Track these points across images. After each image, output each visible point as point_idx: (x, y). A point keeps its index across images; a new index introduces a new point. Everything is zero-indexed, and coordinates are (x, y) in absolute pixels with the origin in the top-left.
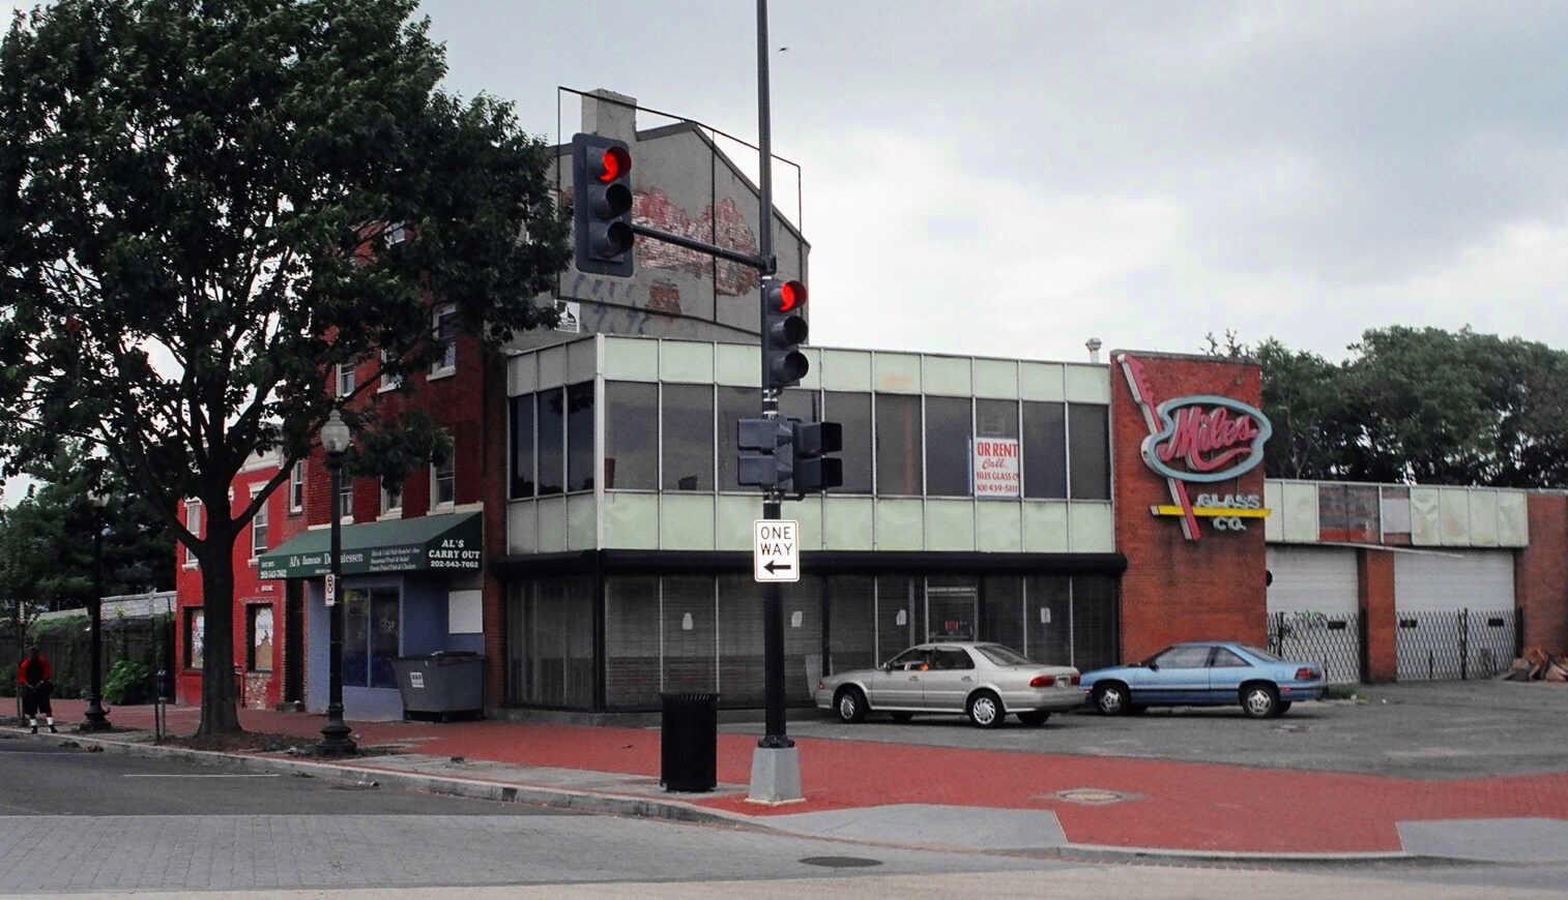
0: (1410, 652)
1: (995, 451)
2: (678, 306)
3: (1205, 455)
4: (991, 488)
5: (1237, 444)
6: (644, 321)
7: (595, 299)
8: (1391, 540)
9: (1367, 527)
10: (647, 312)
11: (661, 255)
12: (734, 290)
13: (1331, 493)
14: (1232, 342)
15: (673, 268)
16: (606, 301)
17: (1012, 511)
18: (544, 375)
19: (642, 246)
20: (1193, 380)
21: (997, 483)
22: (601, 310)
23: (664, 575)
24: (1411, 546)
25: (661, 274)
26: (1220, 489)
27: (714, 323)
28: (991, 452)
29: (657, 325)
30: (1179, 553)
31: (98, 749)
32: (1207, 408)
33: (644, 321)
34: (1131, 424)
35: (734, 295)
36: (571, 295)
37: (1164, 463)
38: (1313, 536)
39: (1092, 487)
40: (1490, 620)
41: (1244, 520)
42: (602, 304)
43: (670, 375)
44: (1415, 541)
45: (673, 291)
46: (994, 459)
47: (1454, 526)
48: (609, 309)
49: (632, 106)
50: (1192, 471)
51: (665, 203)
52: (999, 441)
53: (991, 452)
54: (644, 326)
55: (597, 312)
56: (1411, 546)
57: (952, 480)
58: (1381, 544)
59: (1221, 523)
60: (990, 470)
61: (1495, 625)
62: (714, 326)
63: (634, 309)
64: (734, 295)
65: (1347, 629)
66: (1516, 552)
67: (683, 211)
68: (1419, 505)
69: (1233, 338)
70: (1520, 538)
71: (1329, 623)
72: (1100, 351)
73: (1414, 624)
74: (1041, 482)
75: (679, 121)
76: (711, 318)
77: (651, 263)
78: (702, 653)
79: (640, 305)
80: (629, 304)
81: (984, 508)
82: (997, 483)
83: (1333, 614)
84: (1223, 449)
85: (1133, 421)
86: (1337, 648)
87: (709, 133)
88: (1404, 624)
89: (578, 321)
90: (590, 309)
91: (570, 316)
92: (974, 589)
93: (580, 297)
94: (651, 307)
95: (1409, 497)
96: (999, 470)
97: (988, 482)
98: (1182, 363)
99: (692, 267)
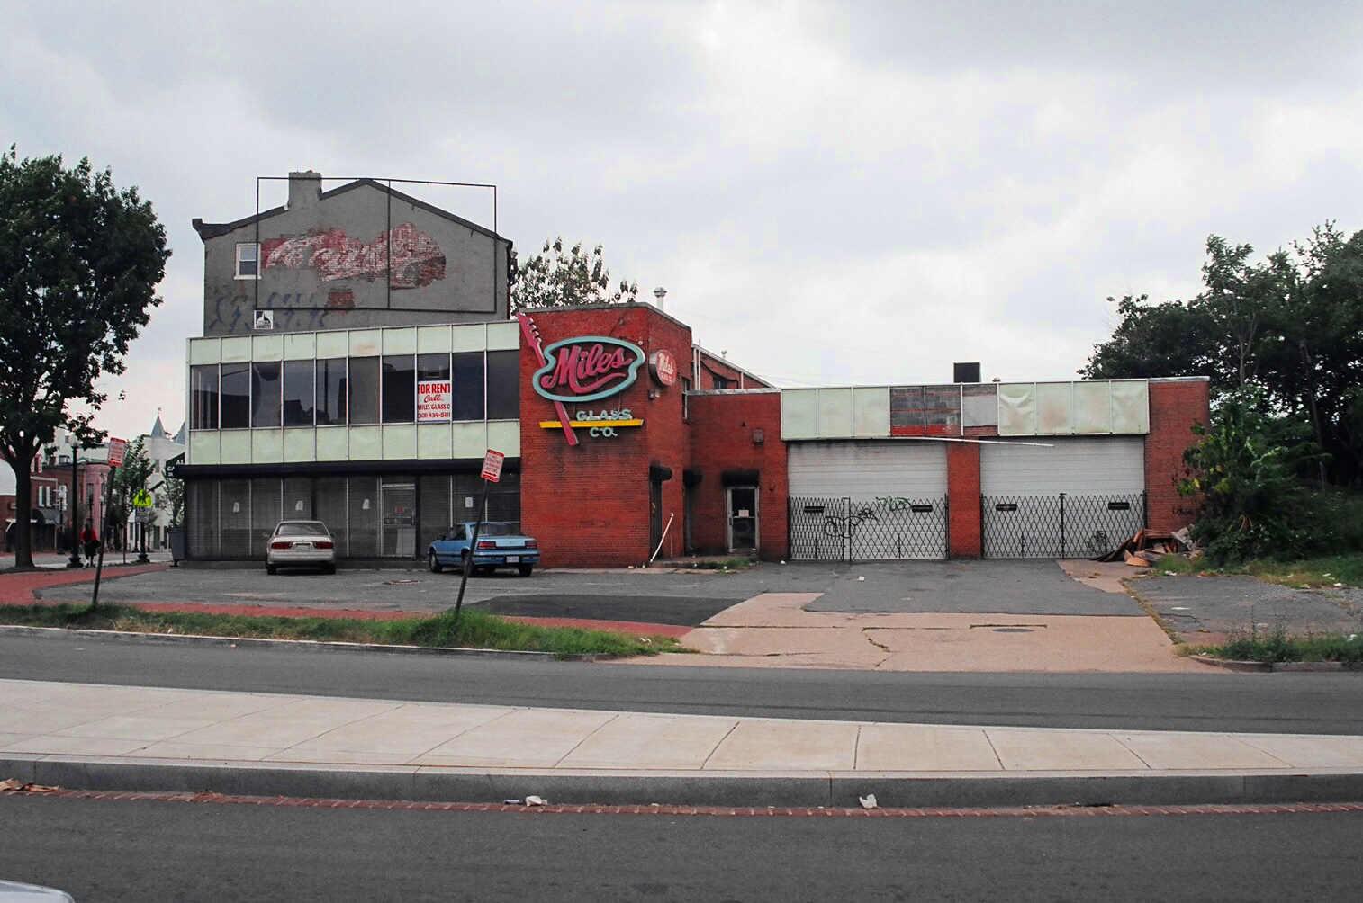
0: (1001, 532)
1: (433, 390)
2: (353, 303)
3: (582, 382)
4: (430, 415)
5: (612, 370)
6: (323, 315)
7: (286, 306)
8: (970, 432)
9: (948, 422)
10: (326, 309)
11: (338, 271)
12: (412, 285)
13: (907, 394)
14: (1329, 231)
15: (349, 278)
16: (293, 306)
17: (445, 430)
18: (420, 346)
19: (322, 268)
20: (583, 325)
21: (435, 411)
22: (290, 313)
23: (221, 480)
24: (999, 438)
25: (339, 285)
26: (596, 406)
27: (388, 309)
28: (431, 390)
29: (333, 317)
30: (568, 457)
31: (1080, 582)
32: (587, 346)
33: (323, 315)
34: (529, 363)
35: (413, 288)
36: (266, 306)
37: (547, 390)
38: (884, 432)
39: (502, 410)
40: (1110, 504)
41: (616, 429)
42: (291, 309)
43: (228, 358)
44: (1001, 432)
45: (349, 293)
46: (433, 395)
47: (1053, 417)
48: (296, 312)
49: (319, 178)
50: (578, 395)
51: (343, 236)
52: (436, 382)
53: (431, 390)
54: (324, 320)
55: (287, 314)
56: (999, 438)
57: (399, 407)
58: (961, 437)
59: (595, 432)
60: (430, 403)
61: (1119, 509)
62: (388, 314)
63: (316, 309)
64: (413, 288)
65: (1107, 503)
66: (1141, 437)
67: (358, 239)
68: (1009, 400)
69: (1331, 226)
70: (1145, 429)
71: (822, 512)
72: (665, 298)
73: (1013, 507)
74: (466, 409)
75: (354, 181)
76: (386, 307)
77: (331, 277)
78: (339, 527)
79: (320, 305)
80: (311, 306)
81: (422, 429)
82: (435, 411)
83: (1118, 494)
84: (600, 375)
85: (531, 360)
86: (1000, 526)
87: (386, 184)
88: (1000, 507)
89: (272, 322)
90: (280, 314)
91: (265, 319)
92: (413, 485)
93: (273, 306)
94: (329, 306)
95: (996, 393)
96: (437, 403)
97: (428, 412)
98: (575, 313)
99: (365, 275)
